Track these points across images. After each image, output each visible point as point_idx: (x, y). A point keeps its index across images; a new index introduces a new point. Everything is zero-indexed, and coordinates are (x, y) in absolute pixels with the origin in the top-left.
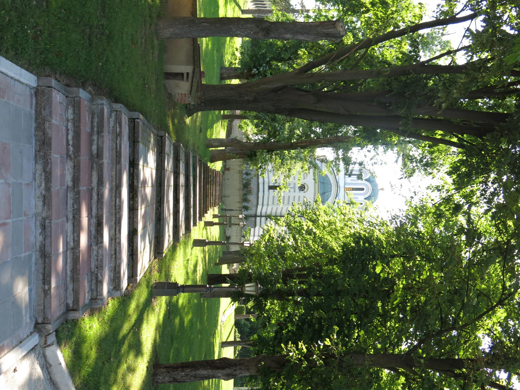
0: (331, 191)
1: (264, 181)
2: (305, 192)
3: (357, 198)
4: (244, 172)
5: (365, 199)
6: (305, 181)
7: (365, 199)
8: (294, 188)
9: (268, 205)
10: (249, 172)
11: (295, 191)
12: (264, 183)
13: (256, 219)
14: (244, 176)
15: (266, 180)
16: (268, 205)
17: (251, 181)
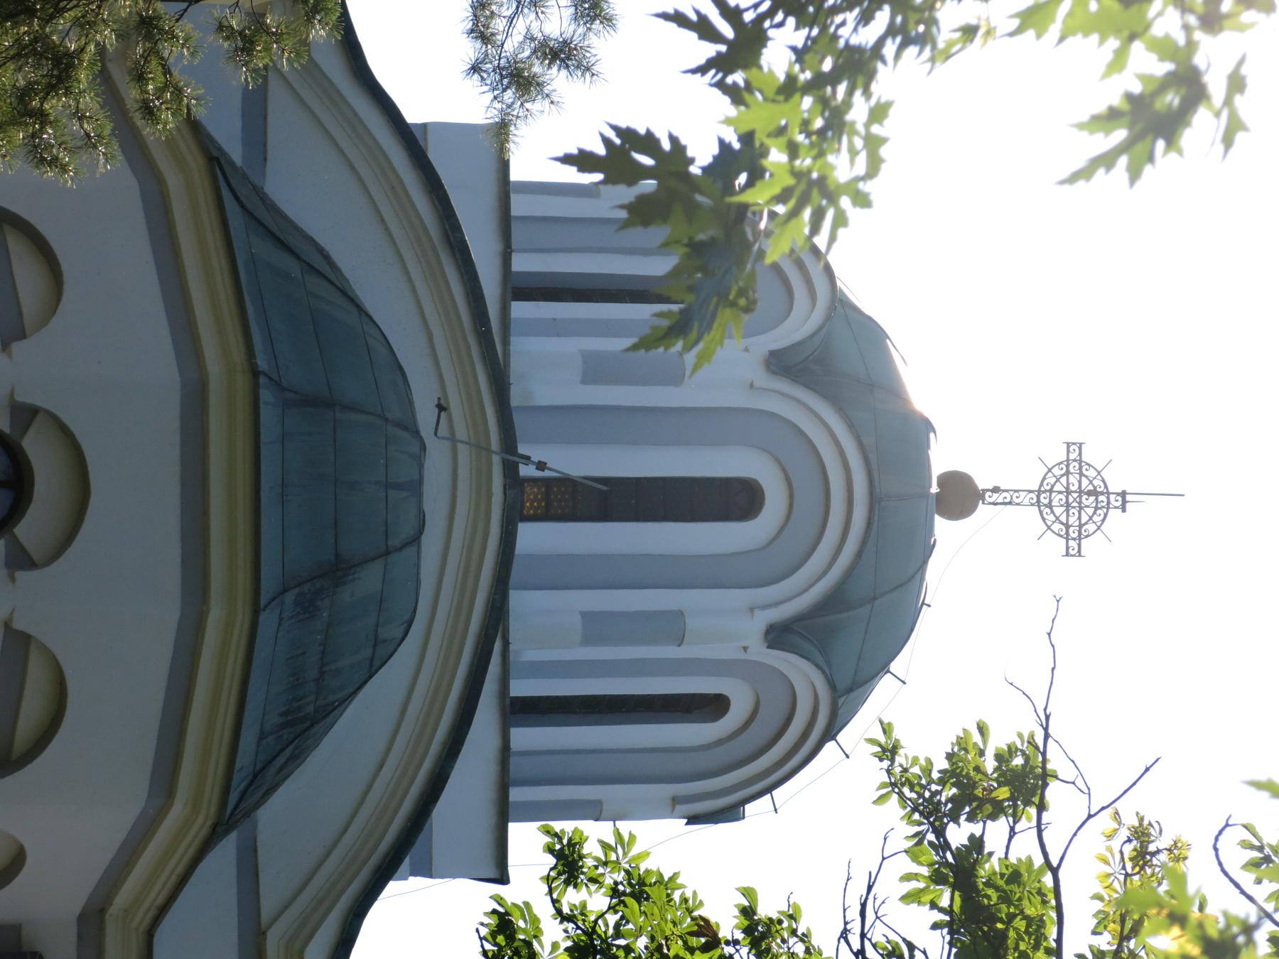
3: (671, 626)
5: (778, 636)
7: (778, 636)
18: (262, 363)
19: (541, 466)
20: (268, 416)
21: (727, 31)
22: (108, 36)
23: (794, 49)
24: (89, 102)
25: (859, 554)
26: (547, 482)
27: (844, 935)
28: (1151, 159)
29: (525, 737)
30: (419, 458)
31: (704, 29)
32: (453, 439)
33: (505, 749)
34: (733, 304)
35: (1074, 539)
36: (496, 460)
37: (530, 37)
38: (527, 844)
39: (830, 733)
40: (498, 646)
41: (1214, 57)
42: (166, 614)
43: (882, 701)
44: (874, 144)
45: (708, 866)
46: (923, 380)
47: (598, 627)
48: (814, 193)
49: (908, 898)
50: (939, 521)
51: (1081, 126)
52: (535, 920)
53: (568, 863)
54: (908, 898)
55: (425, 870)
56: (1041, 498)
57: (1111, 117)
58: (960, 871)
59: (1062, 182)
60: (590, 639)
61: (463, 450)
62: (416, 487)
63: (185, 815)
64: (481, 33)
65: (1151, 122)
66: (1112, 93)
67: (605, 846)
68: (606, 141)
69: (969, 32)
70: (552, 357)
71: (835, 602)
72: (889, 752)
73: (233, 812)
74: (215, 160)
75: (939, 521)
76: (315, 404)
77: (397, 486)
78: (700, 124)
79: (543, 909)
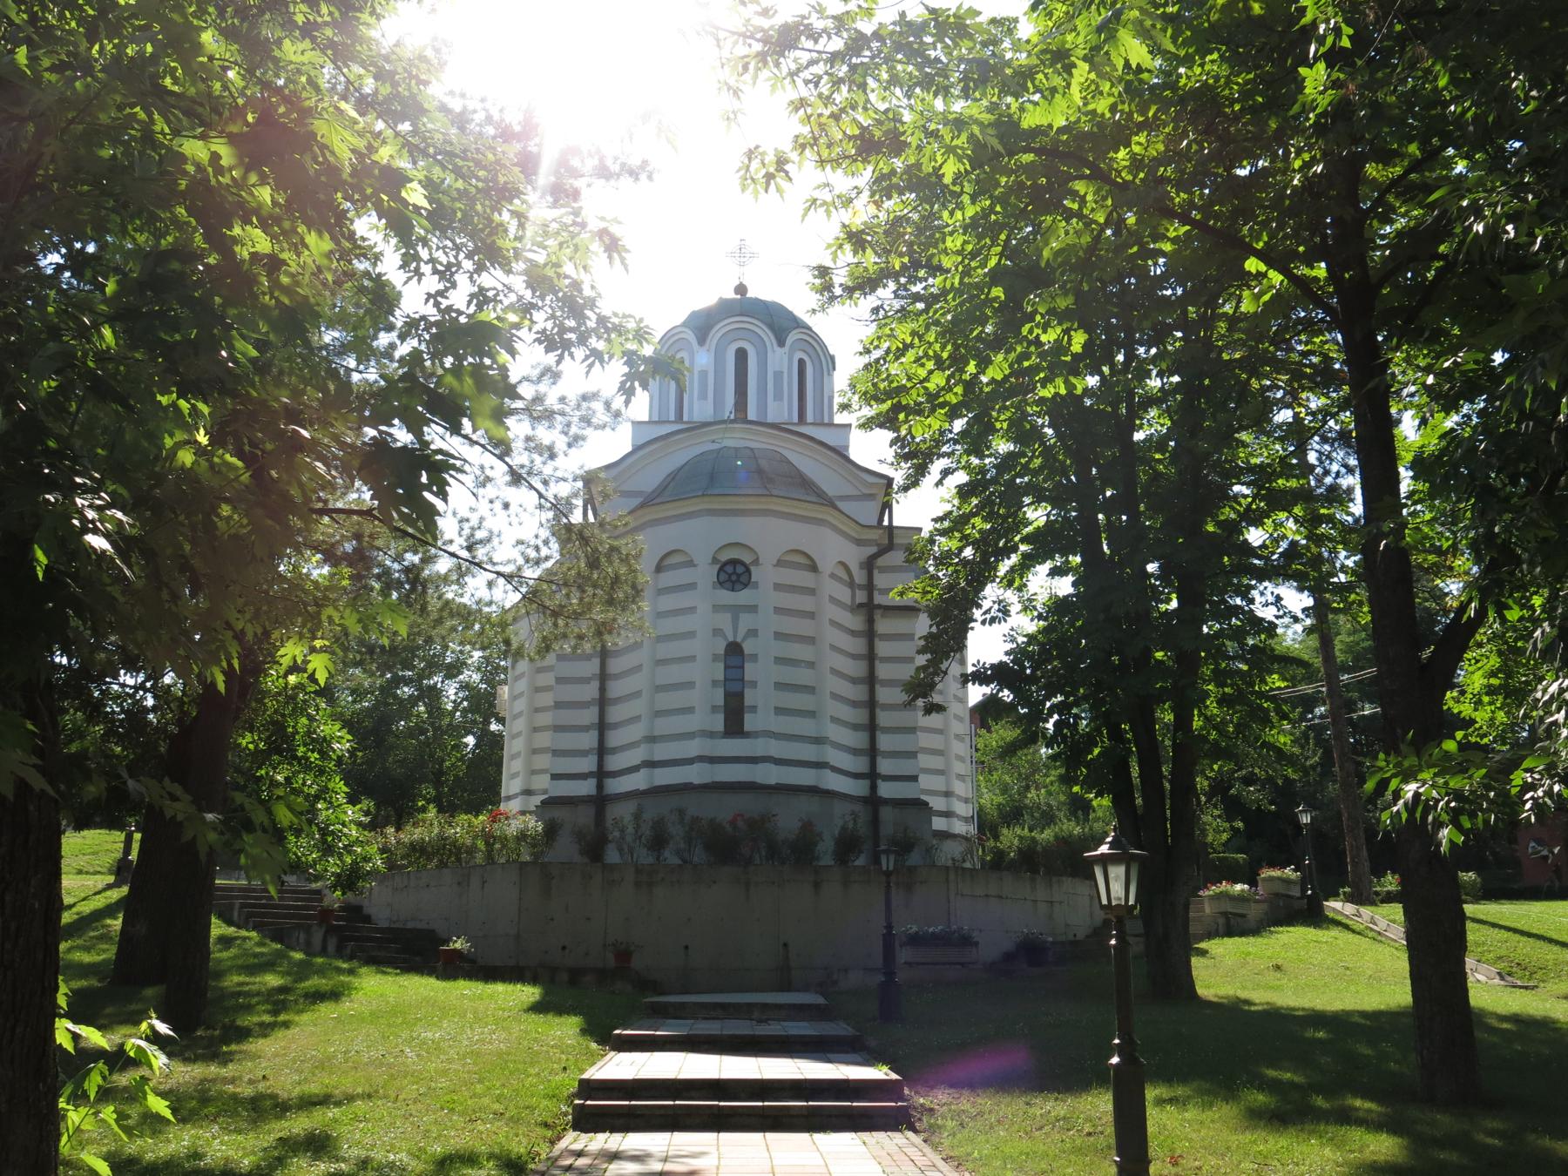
2: (756, 562)
3: (778, 375)
4: (645, 857)
5: (781, 343)
6: (703, 557)
7: (781, 343)
8: (736, 610)
9: (819, 741)
10: (646, 831)
11: (753, 609)
13: (887, 802)
15: (693, 748)
16: (819, 741)
17: (696, 820)
24: (623, 542)
29: (810, 418)
31: (591, 366)
35: (753, 256)
38: (840, 418)
39: (810, 329)
41: (594, 225)
43: (800, 312)
44: (625, 316)
45: (848, 366)
47: (778, 396)
48: (641, 335)
53: (845, 407)
55: (847, 447)
57: (610, 257)
58: (849, 290)
60: (781, 399)
62: (736, 449)
65: (613, 246)
69: (593, 287)
70: (699, 410)
71: (771, 327)
72: (814, 311)
74: (642, 506)
76: (713, 478)
79: (859, 414)
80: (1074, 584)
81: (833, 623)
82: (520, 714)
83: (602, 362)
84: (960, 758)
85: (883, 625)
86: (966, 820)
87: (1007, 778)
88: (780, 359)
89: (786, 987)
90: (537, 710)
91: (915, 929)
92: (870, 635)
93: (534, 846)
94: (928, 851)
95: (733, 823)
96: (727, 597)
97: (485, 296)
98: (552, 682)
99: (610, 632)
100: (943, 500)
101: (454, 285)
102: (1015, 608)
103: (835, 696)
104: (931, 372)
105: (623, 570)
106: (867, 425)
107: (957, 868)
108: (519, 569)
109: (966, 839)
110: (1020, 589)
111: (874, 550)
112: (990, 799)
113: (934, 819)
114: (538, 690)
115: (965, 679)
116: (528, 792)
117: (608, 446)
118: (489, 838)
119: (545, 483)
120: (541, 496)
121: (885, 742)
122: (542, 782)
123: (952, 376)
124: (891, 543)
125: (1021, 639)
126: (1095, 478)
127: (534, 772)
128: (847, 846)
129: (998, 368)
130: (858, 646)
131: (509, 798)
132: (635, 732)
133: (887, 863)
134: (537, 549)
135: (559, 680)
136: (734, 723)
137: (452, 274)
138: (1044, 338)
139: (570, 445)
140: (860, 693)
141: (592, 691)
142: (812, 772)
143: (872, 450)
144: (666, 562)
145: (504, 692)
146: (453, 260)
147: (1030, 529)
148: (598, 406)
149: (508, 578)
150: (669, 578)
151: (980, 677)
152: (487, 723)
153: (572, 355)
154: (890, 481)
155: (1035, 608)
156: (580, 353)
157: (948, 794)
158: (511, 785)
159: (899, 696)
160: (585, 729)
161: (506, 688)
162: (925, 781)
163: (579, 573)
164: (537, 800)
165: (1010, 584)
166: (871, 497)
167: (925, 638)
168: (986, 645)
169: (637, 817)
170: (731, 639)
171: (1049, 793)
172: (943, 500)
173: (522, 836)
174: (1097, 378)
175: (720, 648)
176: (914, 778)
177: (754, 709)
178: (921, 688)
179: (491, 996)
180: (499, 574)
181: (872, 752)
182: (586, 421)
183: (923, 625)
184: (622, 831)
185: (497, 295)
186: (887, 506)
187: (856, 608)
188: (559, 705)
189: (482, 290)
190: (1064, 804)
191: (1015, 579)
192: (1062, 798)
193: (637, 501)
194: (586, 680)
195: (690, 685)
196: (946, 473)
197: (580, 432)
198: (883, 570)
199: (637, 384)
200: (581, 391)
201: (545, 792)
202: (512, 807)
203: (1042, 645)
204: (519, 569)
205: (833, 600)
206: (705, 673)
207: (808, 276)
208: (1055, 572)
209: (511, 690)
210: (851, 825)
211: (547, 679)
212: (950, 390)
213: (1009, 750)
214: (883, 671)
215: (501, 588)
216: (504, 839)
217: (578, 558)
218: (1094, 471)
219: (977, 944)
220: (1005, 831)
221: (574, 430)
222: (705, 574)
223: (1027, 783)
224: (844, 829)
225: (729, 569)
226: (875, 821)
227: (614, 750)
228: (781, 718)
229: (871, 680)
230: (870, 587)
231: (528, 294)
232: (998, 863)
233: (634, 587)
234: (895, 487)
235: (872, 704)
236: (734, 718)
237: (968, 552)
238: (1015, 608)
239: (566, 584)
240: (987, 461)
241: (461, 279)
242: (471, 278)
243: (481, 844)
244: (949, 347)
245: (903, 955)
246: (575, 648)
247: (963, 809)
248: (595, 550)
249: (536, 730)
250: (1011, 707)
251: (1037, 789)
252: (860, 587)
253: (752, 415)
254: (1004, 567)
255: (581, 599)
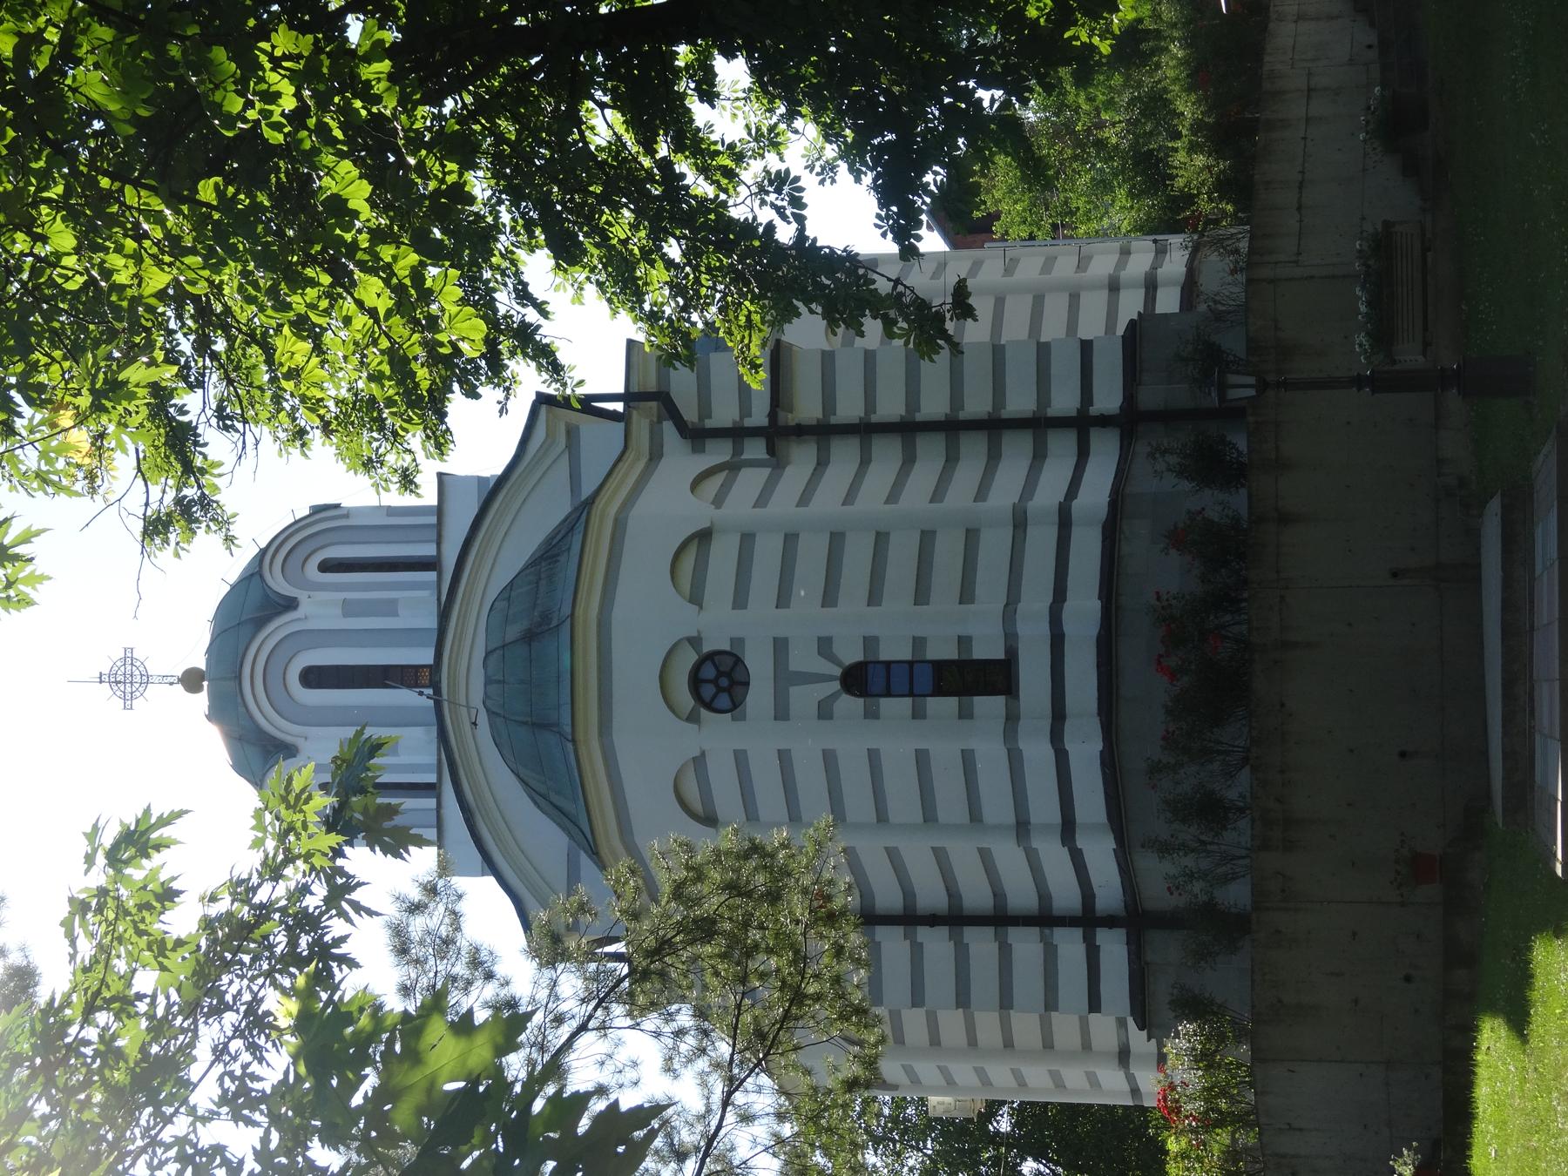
0: (488, 654)
1: (1057, 737)
2: (695, 642)
3: (349, 609)
4: (1239, 835)
5: (291, 604)
6: (687, 740)
7: (291, 604)
8: (785, 678)
9: (1020, 522)
11: (780, 646)
12: (1059, 715)
14: (1238, 788)
15: (1037, 752)
16: (1020, 522)
18: (570, 745)
19: (421, 694)
20: (566, 719)
21: (344, 904)
22: (655, 910)
23: (312, 893)
25: (247, 648)
26: (417, 686)
27: (257, 442)
28: (138, 821)
29: (429, 550)
30: (486, 695)
32: (468, 707)
33: (439, 544)
34: (344, 761)
35: (128, 658)
36: (445, 696)
37: (431, 915)
38: (428, 495)
39: (263, 552)
40: (444, 598)
41: (99, 876)
42: (618, 613)
43: (234, 566)
46: (212, 744)
47: (390, 608)
49: (220, 464)
50: (203, 667)
51: (176, 842)
52: (424, 448)
53: (407, 480)
54: (220, 464)
55: (486, 480)
56: (147, 680)
57: (158, 847)
59: (187, 812)
60: (394, 602)
61: (463, 701)
62: (488, 681)
63: (608, 508)
64: (455, 916)
65: (138, 840)
66: (157, 858)
67: (387, 490)
68: (407, 852)
69: (213, 899)
70: (410, 753)
71: (260, 623)
72: (229, 540)
73: (584, 509)
74: (594, 853)
75: (203, 667)
77: (499, 682)
78: (361, 860)
79: (420, 456)
80: (729, 55)
81: (804, 500)
82: (980, 1072)
83: (350, 887)
84: (1048, 266)
85: (807, 408)
86: (1161, 251)
87: (1083, 180)
88: (320, 605)
89: (1471, 574)
90: (972, 1042)
91: (1361, 338)
92: (824, 432)
93: (1222, 1038)
94: (1218, 317)
95: (1173, 675)
96: (759, 695)
97: (236, 1095)
98: (920, 1013)
99: (829, 898)
100: (578, 299)
101: (219, 1149)
102: (772, 162)
103: (938, 495)
104: (360, 304)
105: (715, 875)
106: (440, 441)
107: (1251, 265)
108: (717, 1066)
109: (1195, 250)
110: (739, 158)
111: (668, 428)
112: (1121, 212)
113: (1159, 310)
114: (935, 1041)
115: (909, 252)
116: (1124, 1056)
117: (488, 914)
118: (1209, 1122)
119: (559, 1020)
120: (583, 1028)
121: (1020, 402)
122: (1104, 1028)
123: (362, 266)
124: (657, 396)
125: (831, 151)
126: (535, 19)
127: (1087, 1046)
128: (1210, 465)
129: (346, 182)
130: (845, 454)
131: (1135, 1091)
132: (1010, 857)
133: (1242, 388)
134: (680, 1033)
135: (917, 1000)
136: (995, 677)
137: (202, 1152)
138: (289, 103)
139: (489, 976)
140: (931, 451)
141: (937, 942)
142: (1077, 534)
143: (484, 433)
144: (698, 807)
145: (939, 1103)
146: (172, 1153)
147: (629, 139)
148: (417, 925)
149: (733, 1085)
150: (727, 798)
151: (903, 230)
152: (996, 1139)
153: (343, 939)
154: (542, 400)
155: (772, 129)
156: (336, 927)
157: (1114, 286)
158: (1108, 1087)
159: (936, 371)
160: (1005, 951)
161: (933, 1100)
162: (1092, 326)
163: (723, 956)
164: (1139, 1039)
165: (730, 174)
166: (572, 433)
167: (832, 324)
168: (846, 216)
169: (1164, 849)
170: (836, 685)
171: (1110, 104)
172: (578, 299)
173: (1205, 1059)
174: (350, 19)
175: (851, 705)
176: (1086, 347)
177: (964, 642)
178: (927, 324)
179: (1499, 1106)
180: (726, 1103)
181: (1039, 425)
182: (445, 945)
183: (808, 331)
184: (1191, 876)
185: (233, 1078)
186: (588, 404)
187: (776, 461)
188: (963, 1000)
189: (224, 1099)
190: (1128, 78)
191: (723, 165)
192: (1117, 80)
193: (585, 860)
194: (917, 951)
195: (922, 758)
196: (523, 295)
197: (464, 959)
198: (705, 408)
199: (387, 824)
200: (391, 959)
201: (1122, 1023)
202: (1150, 1084)
203: (841, 115)
204: (717, 1066)
205: (762, 501)
206: (897, 733)
207: (165, 556)
208: (708, 94)
209: (937, 1091)
210: (1173, 460)
211: (914, 1020)
212: (388, 267)
213: (1036, 173)
214: (891, 407)
215: (753, 1097)
216: (1210, 1094)
217: (695, 958)
218: (521, 21)
219: (1387, 225)
220: (1180, 182)
221: (460, 969)
222: (718, 736)
223: (1089, 144)
224: (1182, 472)
225: (708, 691)
226: (1167, 417)
227: (1044, 896)
228: (980, 590)
229: (908, 429)
230: (737, 434)
231: (230, 1018)
232: (1238, 186)
233: (746, 856)
234: (551, 391)
235: (952, 427)
236: (975, 678)
237: (673, 250)
238: (772, 162)
239: (743, 979)
240: (505, 218)
241: (207, 1136)
242: (205, 1120)
243: (1223, 1137)
244: (309, 272)
245: (1410, 356)
246: (858, 962)
247: (1141, 259)
248: (681, 927)
249: (1008, 1044)
250: (957, 170)
251: (1101, 125)
252: (737, 451)
253: (425, 656)
254: (703, 188)
255: (770, 951)
